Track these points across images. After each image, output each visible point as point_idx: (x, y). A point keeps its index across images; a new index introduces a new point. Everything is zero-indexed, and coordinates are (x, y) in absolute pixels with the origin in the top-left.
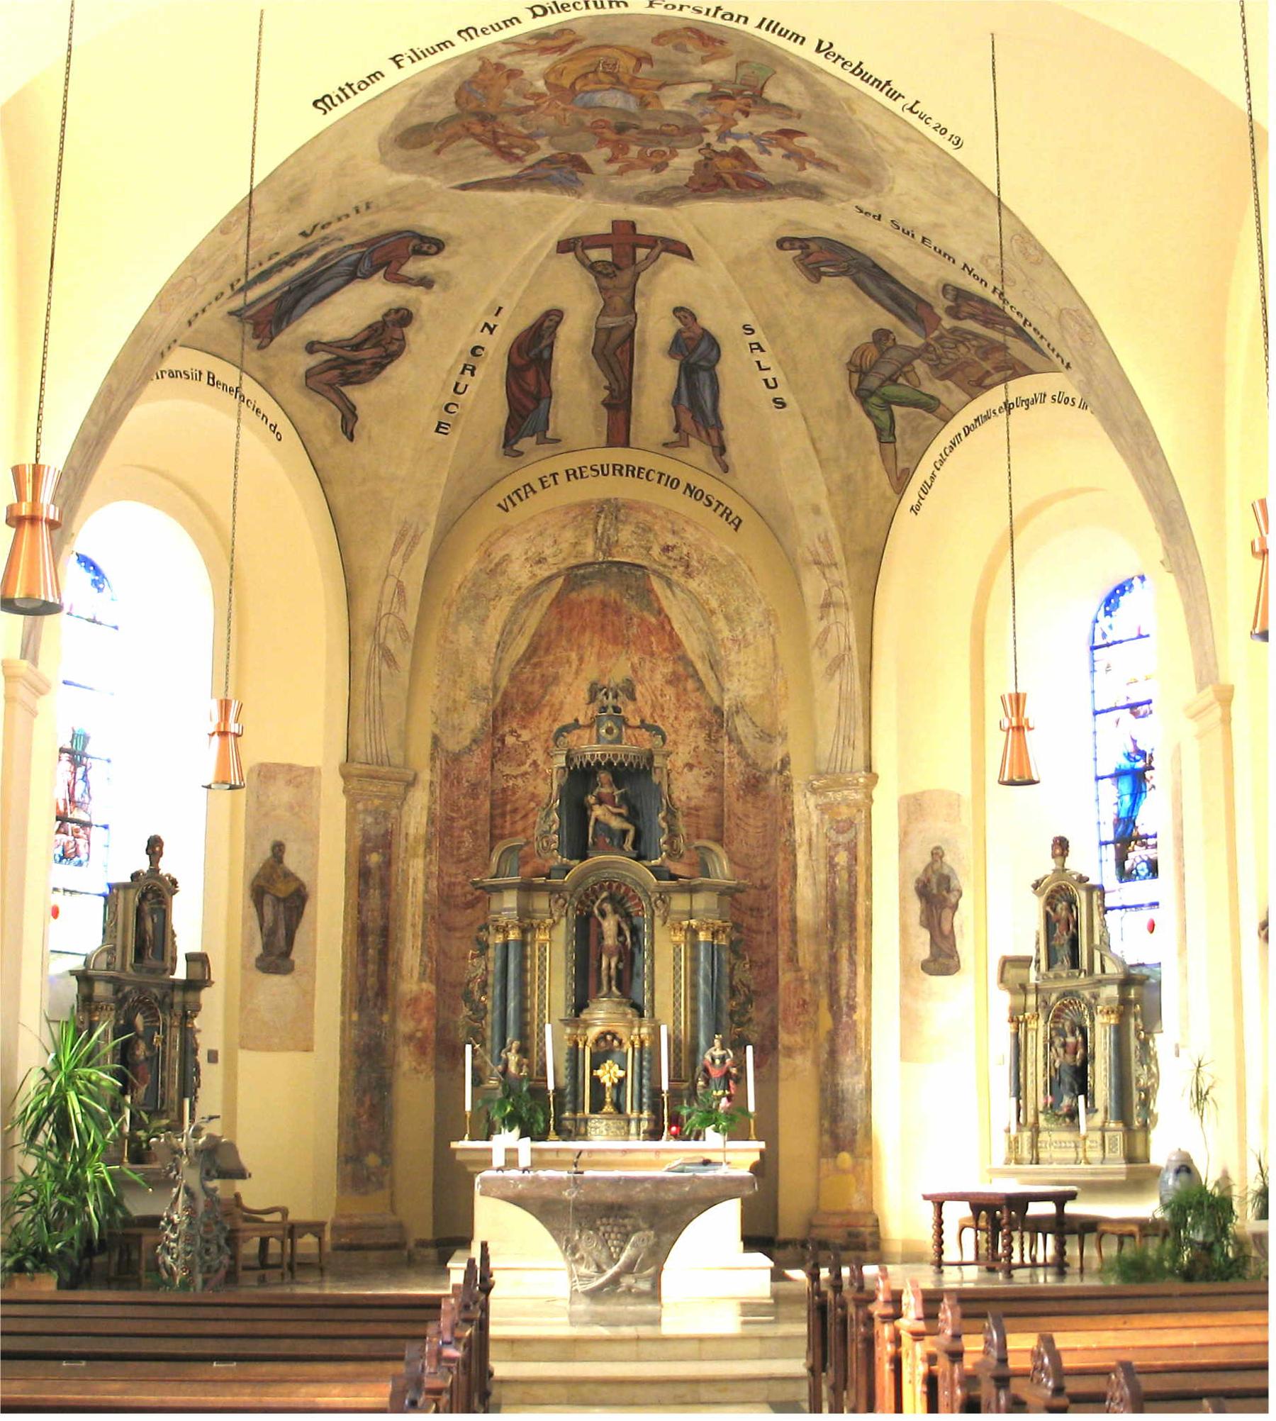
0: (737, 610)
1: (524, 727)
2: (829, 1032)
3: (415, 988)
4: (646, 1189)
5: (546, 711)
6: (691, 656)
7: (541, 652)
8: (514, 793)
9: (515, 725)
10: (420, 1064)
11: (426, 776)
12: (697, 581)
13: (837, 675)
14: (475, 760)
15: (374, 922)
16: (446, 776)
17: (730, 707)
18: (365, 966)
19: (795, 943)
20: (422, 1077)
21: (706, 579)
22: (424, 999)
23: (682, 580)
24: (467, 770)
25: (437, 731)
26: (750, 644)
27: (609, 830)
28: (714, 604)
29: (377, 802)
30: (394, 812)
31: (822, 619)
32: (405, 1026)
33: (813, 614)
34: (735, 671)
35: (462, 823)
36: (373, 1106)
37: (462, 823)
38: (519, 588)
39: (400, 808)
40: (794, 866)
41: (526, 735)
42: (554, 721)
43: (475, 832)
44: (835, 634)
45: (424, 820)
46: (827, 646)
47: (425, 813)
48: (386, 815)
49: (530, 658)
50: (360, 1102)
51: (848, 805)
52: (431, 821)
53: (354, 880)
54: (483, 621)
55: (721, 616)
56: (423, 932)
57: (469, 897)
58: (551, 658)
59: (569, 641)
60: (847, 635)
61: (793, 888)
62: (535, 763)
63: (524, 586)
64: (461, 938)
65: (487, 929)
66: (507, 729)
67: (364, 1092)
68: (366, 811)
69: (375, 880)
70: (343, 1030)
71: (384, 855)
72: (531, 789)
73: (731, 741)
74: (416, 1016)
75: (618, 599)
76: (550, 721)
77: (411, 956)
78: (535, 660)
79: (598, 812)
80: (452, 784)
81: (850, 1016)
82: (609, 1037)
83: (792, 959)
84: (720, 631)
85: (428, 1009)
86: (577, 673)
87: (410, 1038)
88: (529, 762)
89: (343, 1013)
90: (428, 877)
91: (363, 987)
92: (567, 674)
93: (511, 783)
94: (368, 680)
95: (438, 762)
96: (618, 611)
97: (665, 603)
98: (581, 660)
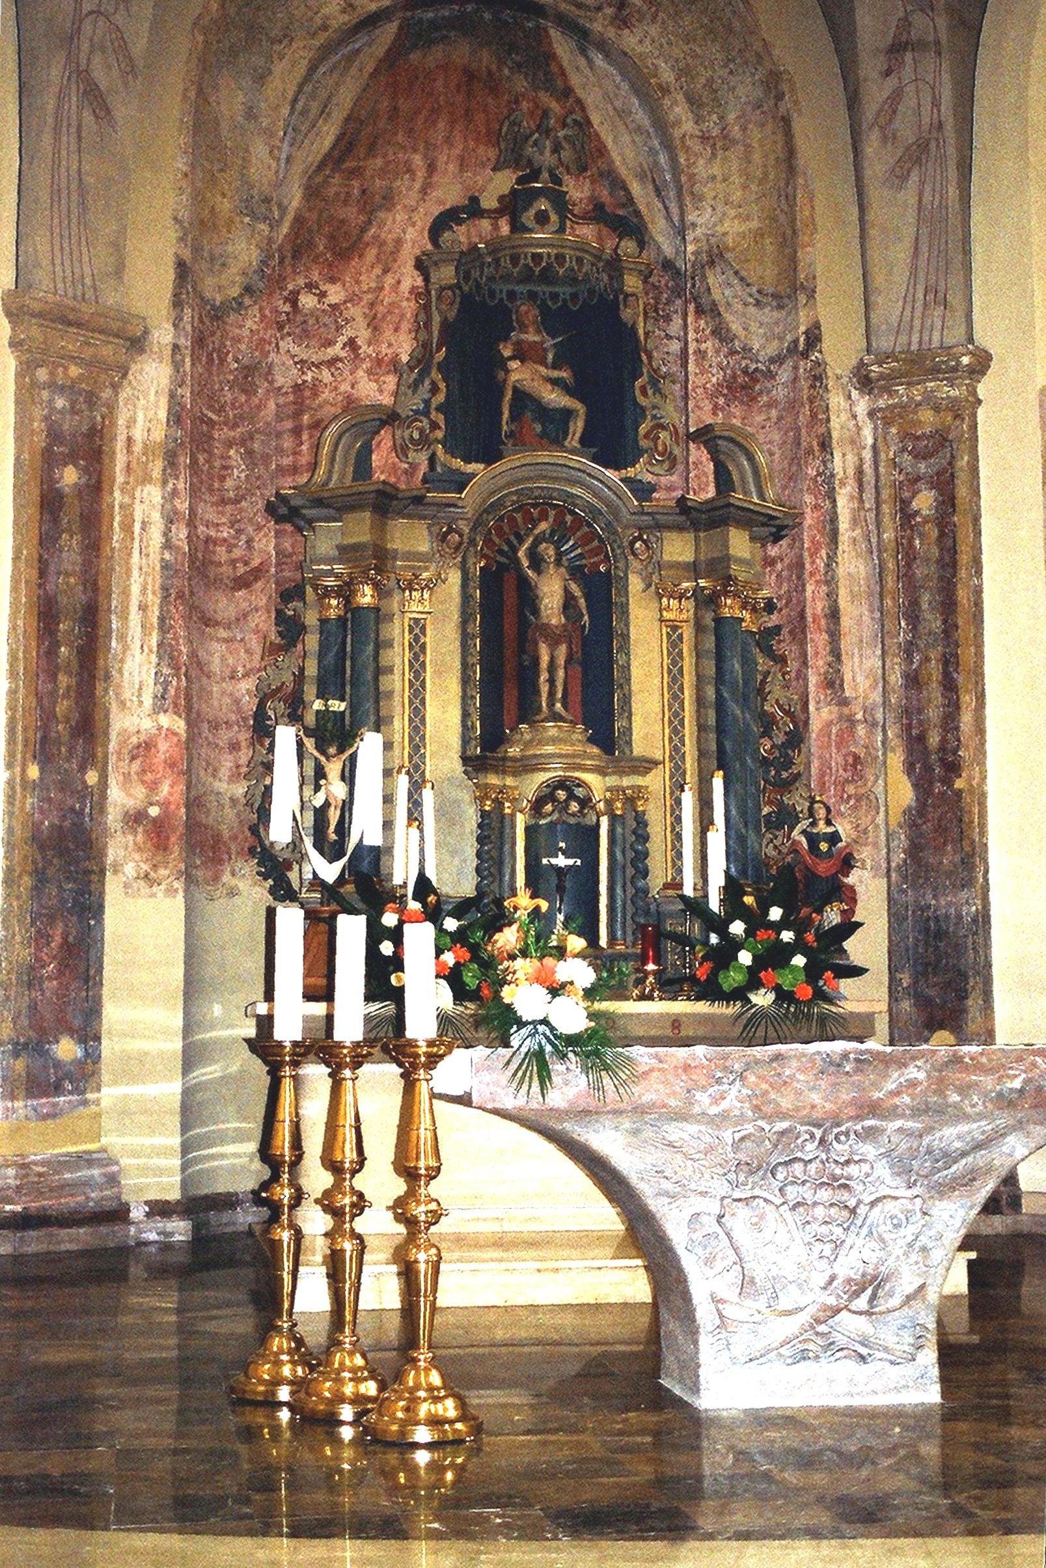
0: (710, 81)
1: (333, 280)
2: (907, 811)
3: (147, 724)
4: (913, 1084)
5: (371, 254)
6: (623, 172)
7: (362, 152)
8: (315, 394)
9: (315, 276)
10: (155, 867)
11: (163, 335)
12: (639, 32)
13: (914, 177)
14: (249, 323)
15: (68, 588)
16: (199, 341)
17: (696, 253)
18: (53, 678)
19: (836, 654)
20: (159, 890)
21: (654, 30)
22: (163, 746)
23: (611, 33)
24: (237, 340)
25: (187, 254)
26: (734, 142)
27: (543, 412)
28: (667, 75)
29: (74, 371)
30: (106, 394)
31: (888, 73)
32: (120, 797)
33: (870, 67)
34: (708, 191)
35: (228, 434)
36: (66, 945)
37: (228, 434)
38: (325, 28)
39: (116, 387)
40: (834, 519)
41: (335, 294)
42: (386, 271)
43: (250, 453)
44: (913, 103)
45: (163, 415)
46: (897, 124)
47: (164, 402)
48: (91, 399)
49: (341, 160)
50: (41, 939)
51: (937, 409)
52: (176, 417)
53: (33, 511)
54: (261, 78)
55: (680, 97)
56: (162, 619)
57: (241, 569)
58: (379, 162)
59: (410, 132)
60: (936, 104)
61: (832, 558)
62: (352, 343)
63: (334, 24)
64: (226, 641)
65: (302, 597)
66: (301, 282)
67: (52, 919)
68: (52, 385)
69: (70, 516)
70: (10, 799)
71: (85, 471)
72: (345, 387)
73: (699, 312)
74: (149, 776)
75: (494, 67)
76: (378, 271)
77: (136, 669)
78: (349, 164)
79: (519, 374)
80: (210, 360)
81: (948, 782)
82: (561, 794)
83: (833, 683)
84: (678, 123)
85: (171, 764)
86: (424, 191)
87: (135, 818)
88: (342, 339)
89: (9, 766)
90: (170, 519)
91: (48, 717)
92: (408, 190)
93: (309, 377)
94: (57, 138)
95: (188, 311)
96: (494, 86)
97: (575, 80)
98: (431, 168)
